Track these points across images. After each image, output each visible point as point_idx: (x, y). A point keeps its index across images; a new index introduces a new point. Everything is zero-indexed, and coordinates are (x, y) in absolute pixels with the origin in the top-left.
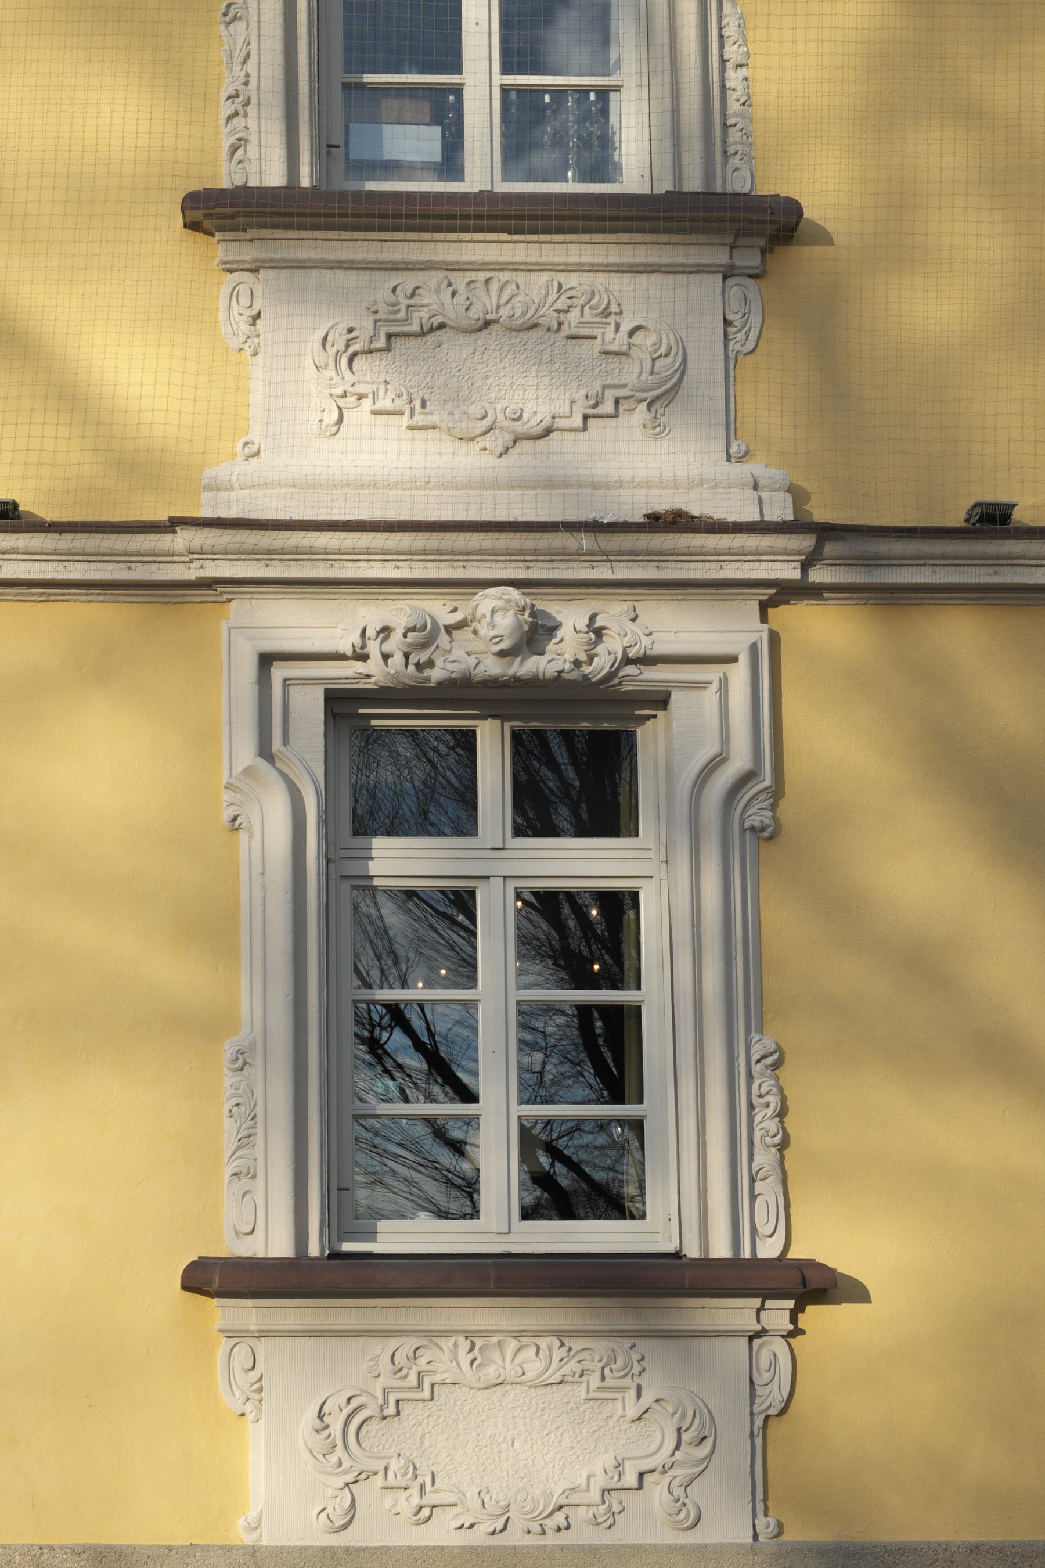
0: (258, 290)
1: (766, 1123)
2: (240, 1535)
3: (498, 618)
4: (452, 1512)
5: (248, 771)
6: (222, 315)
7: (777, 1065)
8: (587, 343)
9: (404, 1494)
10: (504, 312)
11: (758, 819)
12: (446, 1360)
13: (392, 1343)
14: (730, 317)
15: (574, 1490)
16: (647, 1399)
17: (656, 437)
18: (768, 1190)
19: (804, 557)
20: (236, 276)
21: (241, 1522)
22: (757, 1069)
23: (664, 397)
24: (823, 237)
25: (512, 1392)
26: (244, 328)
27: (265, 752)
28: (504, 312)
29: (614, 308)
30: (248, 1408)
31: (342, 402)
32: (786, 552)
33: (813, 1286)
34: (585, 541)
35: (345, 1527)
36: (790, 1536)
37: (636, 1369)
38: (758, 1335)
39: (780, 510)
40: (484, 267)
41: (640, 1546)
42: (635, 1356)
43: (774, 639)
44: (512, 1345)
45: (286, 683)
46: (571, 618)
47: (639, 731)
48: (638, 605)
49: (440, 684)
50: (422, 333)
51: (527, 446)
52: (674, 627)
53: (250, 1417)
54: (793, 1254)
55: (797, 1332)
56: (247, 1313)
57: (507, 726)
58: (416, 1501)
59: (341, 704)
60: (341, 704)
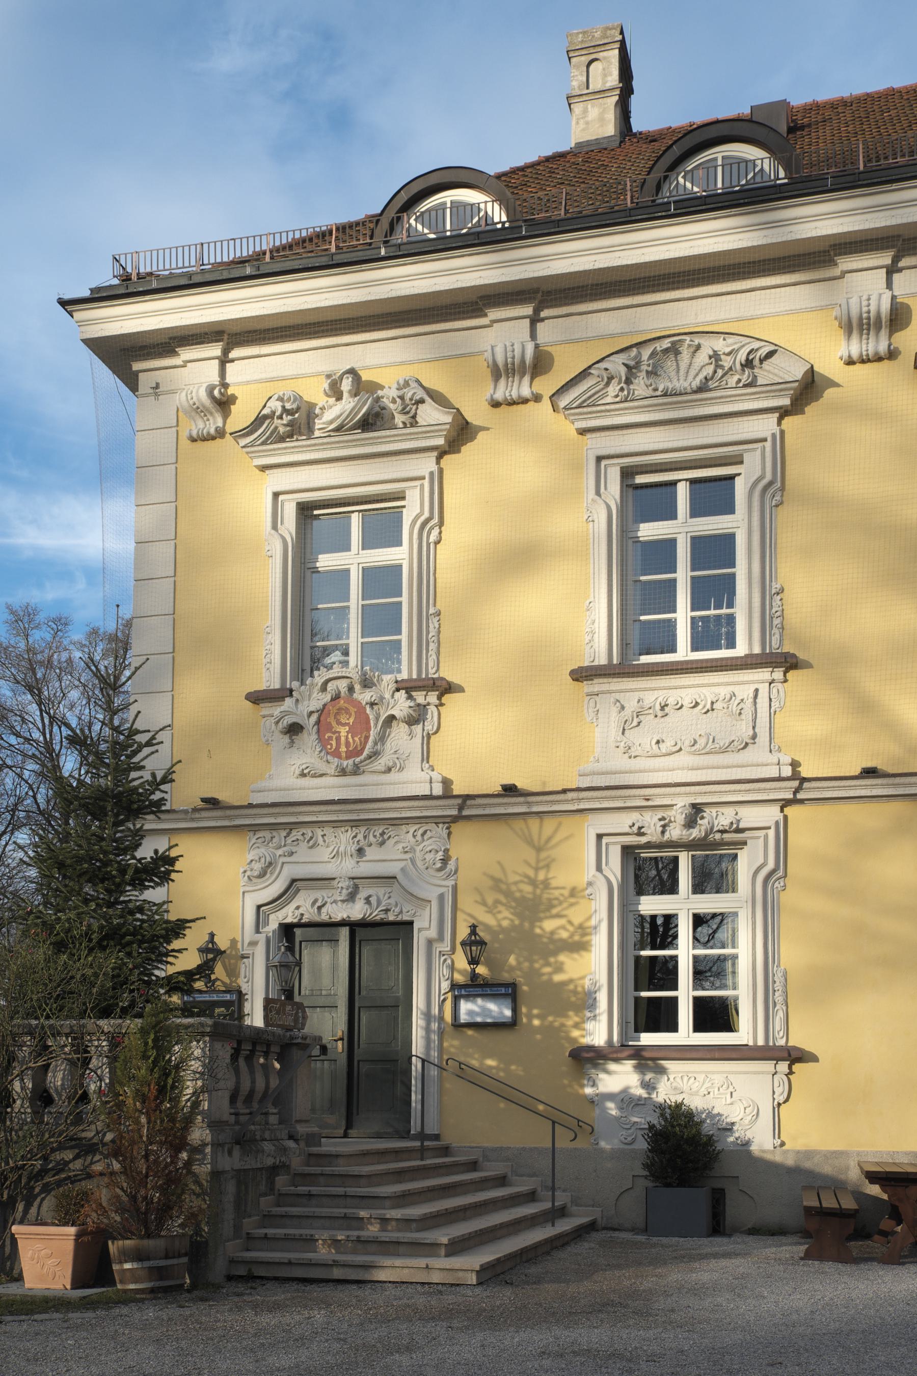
19: (792, 392)
27: (598, 493)
45: (607, 844)
57: (691, 853)
60: (627, 851)
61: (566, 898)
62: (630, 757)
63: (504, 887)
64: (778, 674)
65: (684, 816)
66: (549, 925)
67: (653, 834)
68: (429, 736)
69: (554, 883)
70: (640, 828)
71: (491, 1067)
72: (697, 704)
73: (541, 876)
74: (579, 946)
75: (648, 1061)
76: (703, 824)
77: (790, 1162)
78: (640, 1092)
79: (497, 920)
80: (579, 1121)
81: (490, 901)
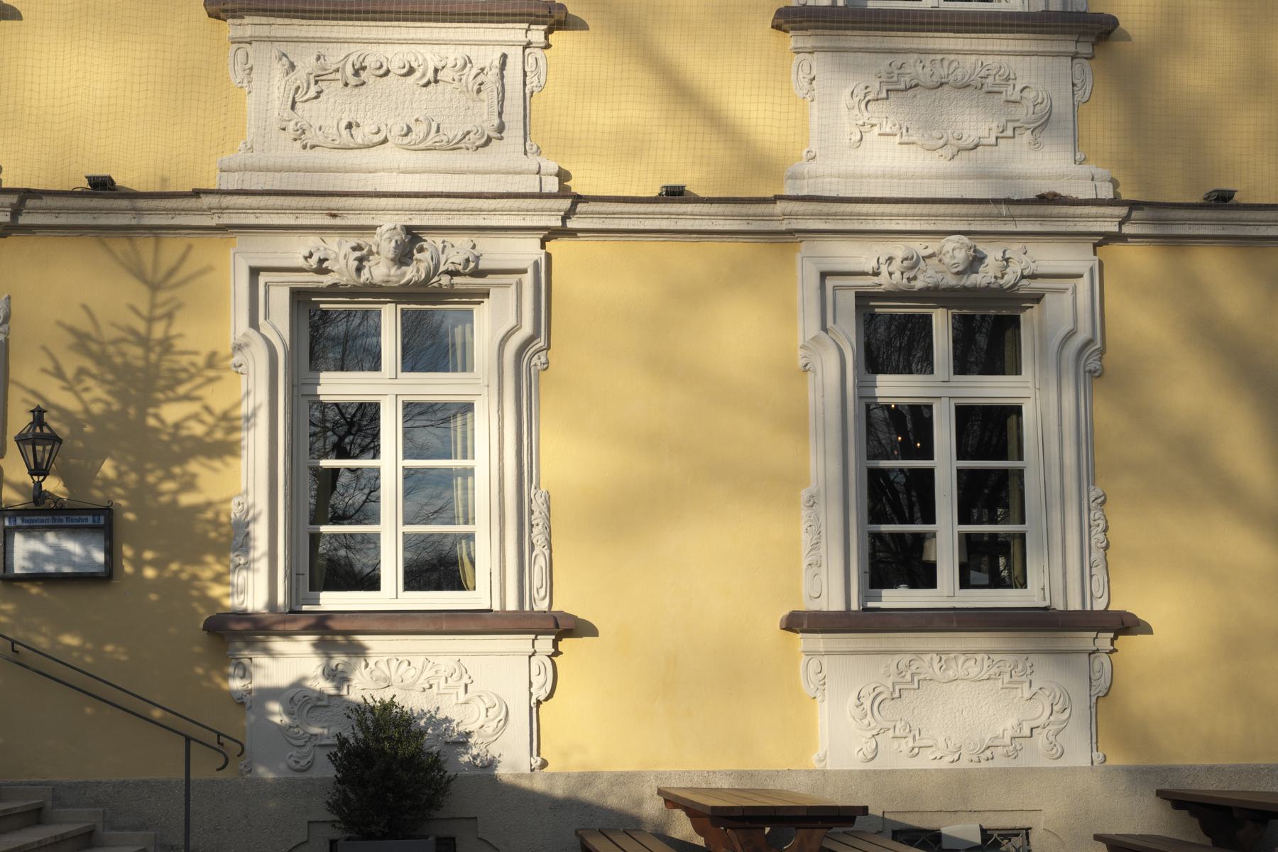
0: (814, 65)
1: (1097, 536)
2: (814, 763)
3: (956, 253)
4: (930, 750)
5: (814, 339)
6: (793, 77)
7: (1103, 503)
8: (997, 96)
9: (903, 741)
10: (952, 78)
11: (1094, 364)
12: (929, 665)
13: (898, 657)
14: (1076, 81)
15: (996, 737)
16: (1035, 688)
17: (1036, 150)
18: (1099, 572)
20: (801, 56)
21: (815, 757)
22: (1093, 505)
23: (1043, 124)
24: (1126, 37)
25: (962, 685)
26: (806, 85)
27: (824, 328)
28: (952, 78)
29: (1012, 76)
30: (818, 694)
31: (862, 129)
32: (1112, 217)
33: (1126, 625)
34: (1004, 209)
35: (873, 759)
36: (1112, 761)
37: (1029, 671)
38: (1094, 652)
39: (1106, 192)
40: (941, 52)
41: (1032, 769)
42: (1028, 664)
43: (549, 257)
44: (962, 658)
46: (993, 253)
47: (1022, 316)
48: (1028, 246)
49: (921, 290)
50: (906, 90)
51: (965, 154)
52: (1050, 257)
53: (819, 699)
54: (555, 608)
55: (557, 653)
56: (819, 641)
57: (400, 307)
58: (911, 744)
59: (863, 299)
60: (863, 299)
61: (200, 372)
62: (305, 147)
63: (94, 347)
64: (537, 34)
65: (393, 244)
66: (172, 413)
67: (342, 272)
68: (539, 703)
69: (179, 345)
70: (321, 261)
71: (70, 648)
72: (411, 71)
73: (158, 331)
74: (226, 449)
75: (335, 636)
76: (423, 260)
77: (559, 791)
78: (327, 687)
79: (78, 399)
80: (219, 734)
81: (70, 372)
